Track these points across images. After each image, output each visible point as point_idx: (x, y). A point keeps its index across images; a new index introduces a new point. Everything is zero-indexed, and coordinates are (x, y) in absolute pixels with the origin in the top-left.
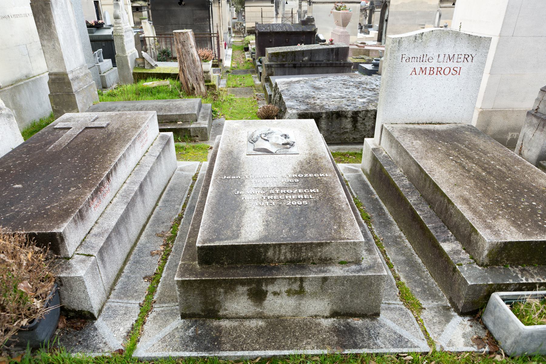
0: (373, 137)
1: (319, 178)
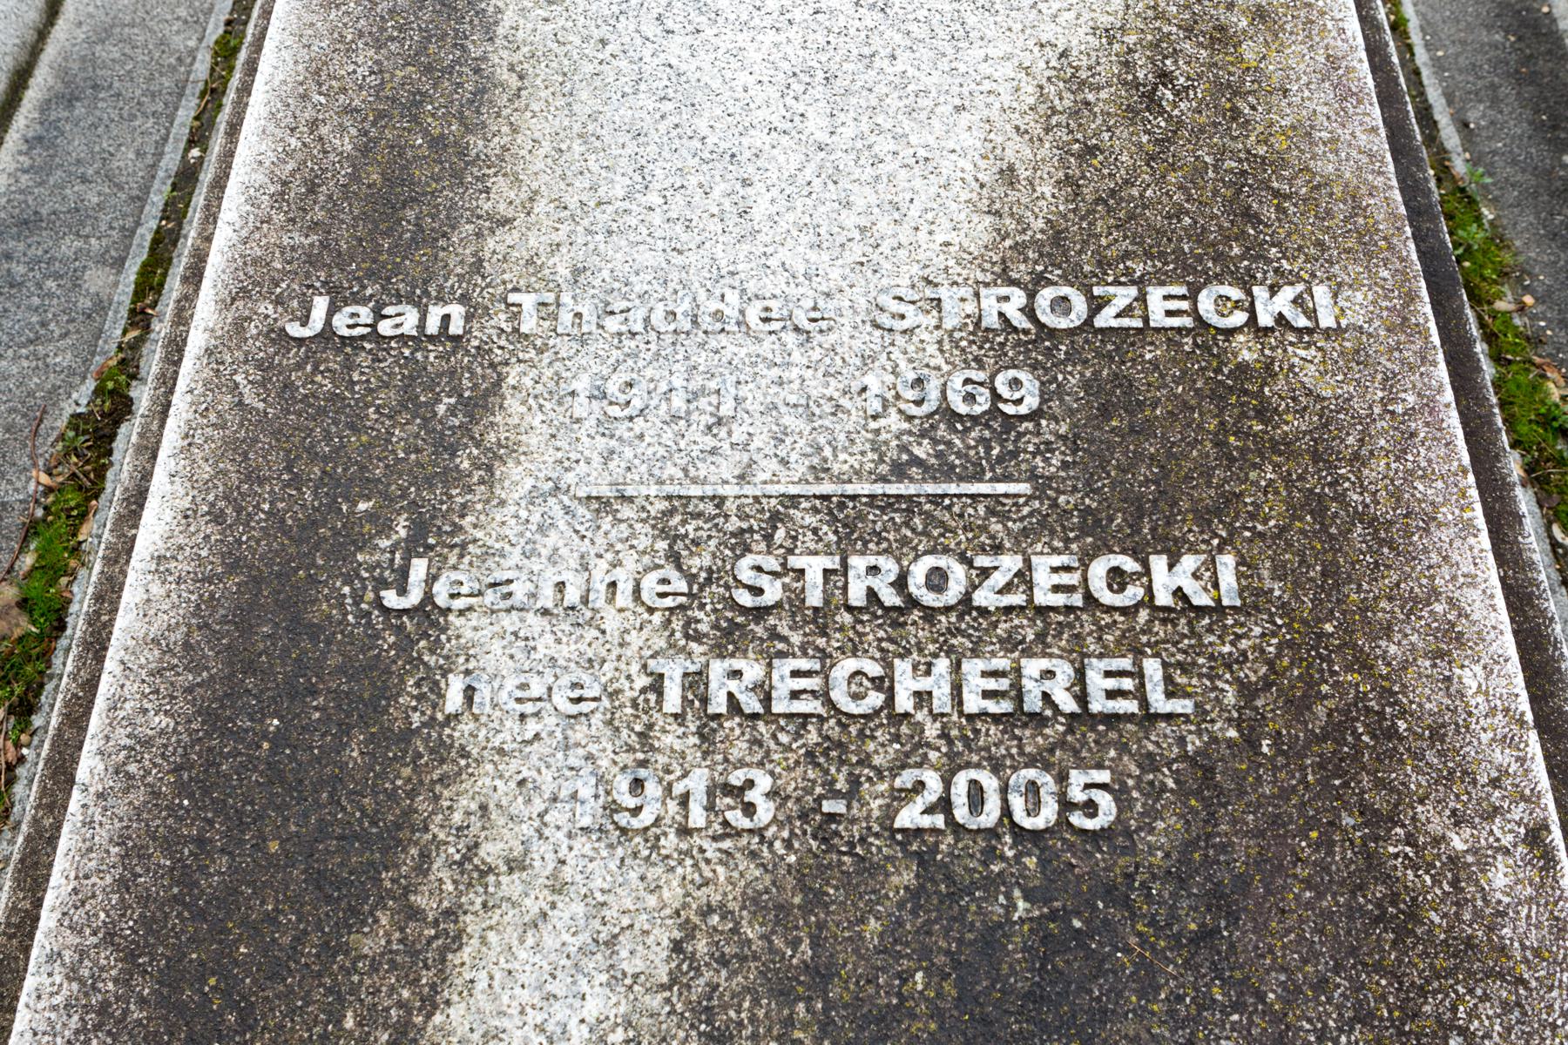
0: (930, 693)
1: (1246, 351)
